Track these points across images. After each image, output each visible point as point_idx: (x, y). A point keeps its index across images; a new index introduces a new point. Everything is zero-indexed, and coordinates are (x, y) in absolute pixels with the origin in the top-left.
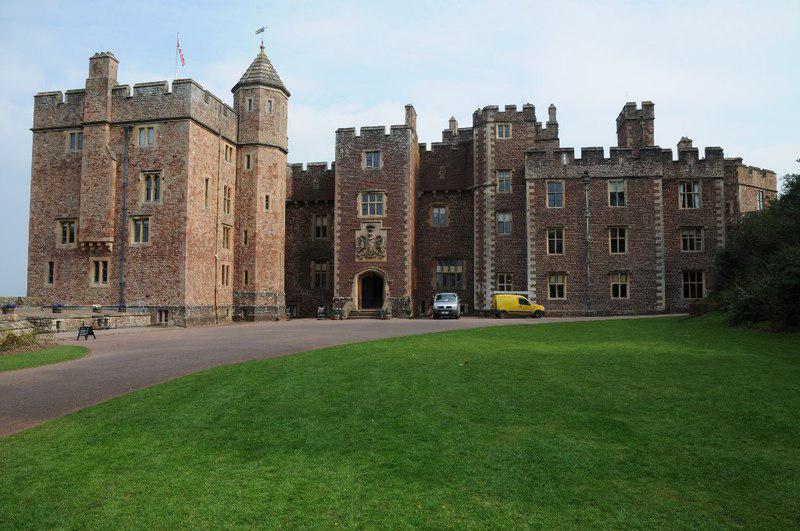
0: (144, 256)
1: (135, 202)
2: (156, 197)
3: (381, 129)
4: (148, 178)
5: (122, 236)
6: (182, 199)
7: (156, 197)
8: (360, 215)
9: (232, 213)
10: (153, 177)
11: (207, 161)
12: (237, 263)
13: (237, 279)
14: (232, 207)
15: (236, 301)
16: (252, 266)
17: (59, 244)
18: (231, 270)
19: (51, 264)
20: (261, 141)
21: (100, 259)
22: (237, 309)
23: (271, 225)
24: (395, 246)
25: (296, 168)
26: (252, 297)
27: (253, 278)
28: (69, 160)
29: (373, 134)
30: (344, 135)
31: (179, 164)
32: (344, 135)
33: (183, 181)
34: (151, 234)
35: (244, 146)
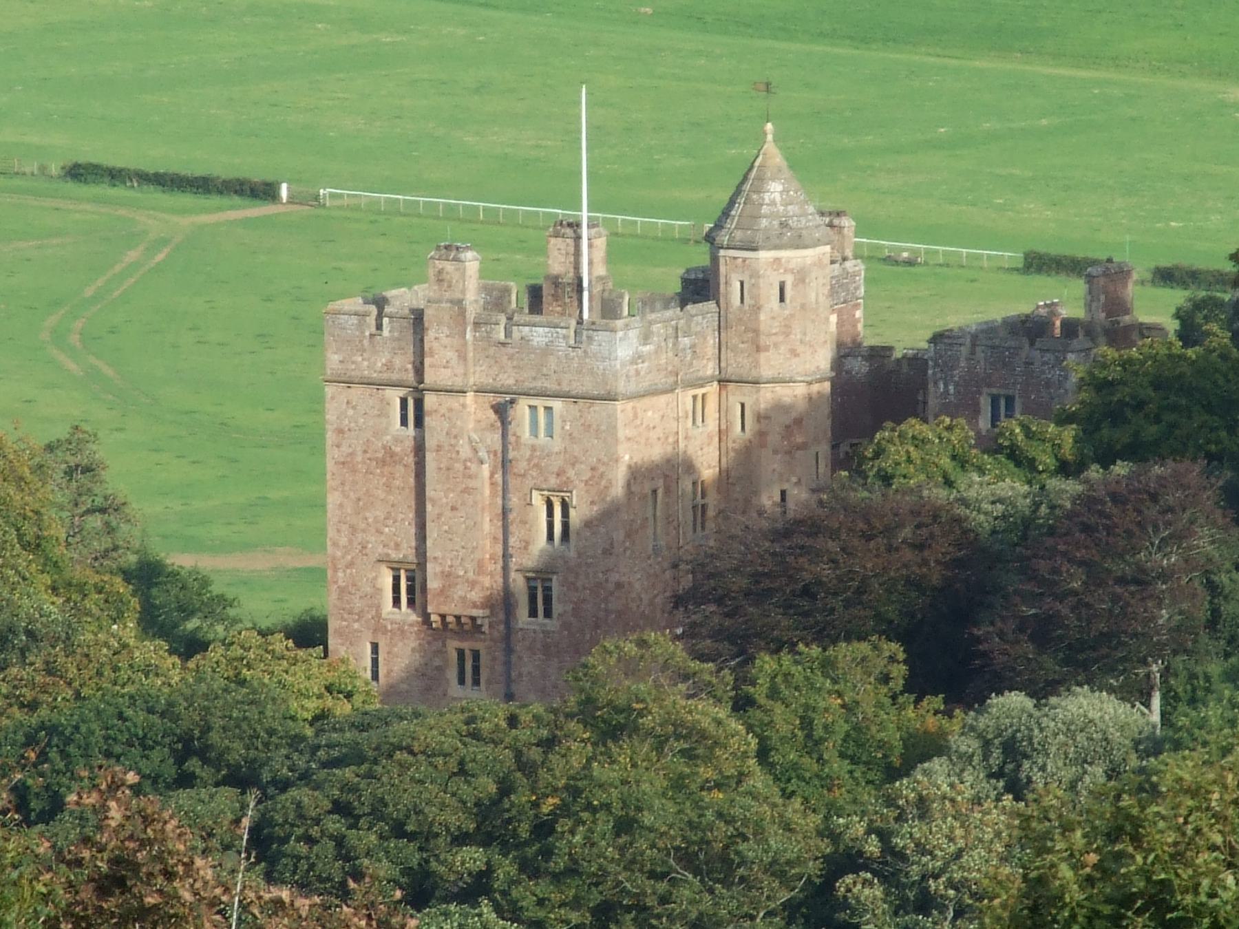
0: (546, 648)
1: (526, 544)
19: (375, 648)
21: (466, 645)
28: (398, 450)
34: (557, 608)
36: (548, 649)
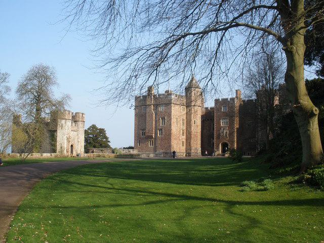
2: (164, 124)
3: (227, 99)
4: (162, 119)
5: (156, 134)
6: (170, 125)
7: (164, 124)
8: (222, 125)
9: (185, 126)
10: (163, 119)
11: (177, 112)
12: (187, 140)
13: (186, 145)
14: (185, 124)
15: (186, 151)
16: (190, 141)
17: (141, 136)
18: (185, 142)
20: (240, 23)
22: (187, 153)
23: (197, 128)
24: (231, 134)
25: (207, 108)
26: (191, 150)
27: (140, 188)
29: (225, 101)
30: (217, 101)
31: (170, 115)
32: (217, 101)
33: (171, 120)
35: (188, 105)
36: (162, 139)
